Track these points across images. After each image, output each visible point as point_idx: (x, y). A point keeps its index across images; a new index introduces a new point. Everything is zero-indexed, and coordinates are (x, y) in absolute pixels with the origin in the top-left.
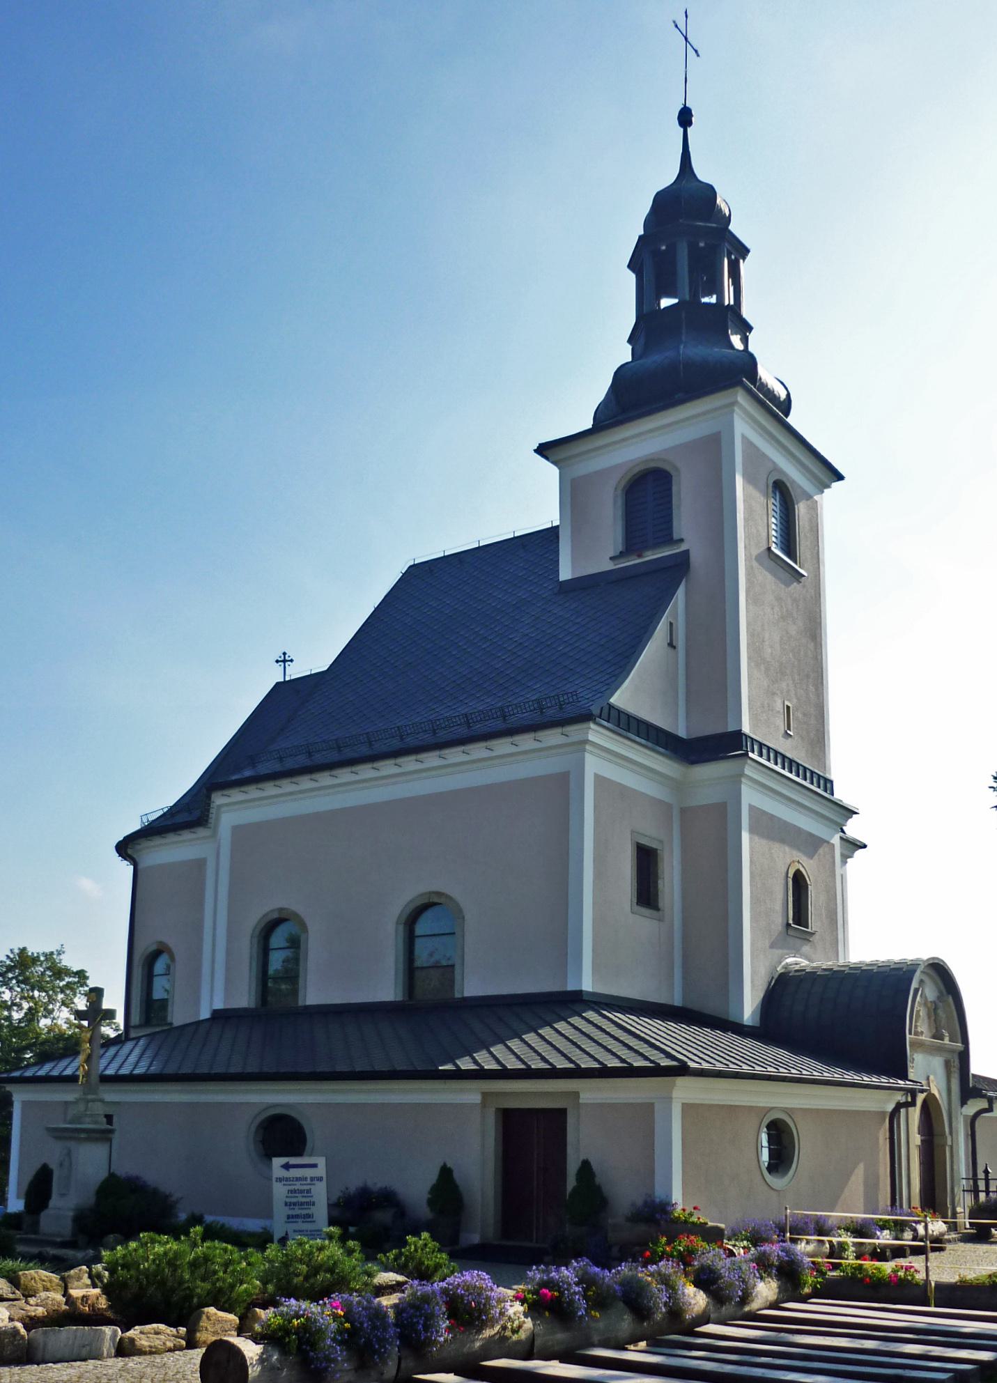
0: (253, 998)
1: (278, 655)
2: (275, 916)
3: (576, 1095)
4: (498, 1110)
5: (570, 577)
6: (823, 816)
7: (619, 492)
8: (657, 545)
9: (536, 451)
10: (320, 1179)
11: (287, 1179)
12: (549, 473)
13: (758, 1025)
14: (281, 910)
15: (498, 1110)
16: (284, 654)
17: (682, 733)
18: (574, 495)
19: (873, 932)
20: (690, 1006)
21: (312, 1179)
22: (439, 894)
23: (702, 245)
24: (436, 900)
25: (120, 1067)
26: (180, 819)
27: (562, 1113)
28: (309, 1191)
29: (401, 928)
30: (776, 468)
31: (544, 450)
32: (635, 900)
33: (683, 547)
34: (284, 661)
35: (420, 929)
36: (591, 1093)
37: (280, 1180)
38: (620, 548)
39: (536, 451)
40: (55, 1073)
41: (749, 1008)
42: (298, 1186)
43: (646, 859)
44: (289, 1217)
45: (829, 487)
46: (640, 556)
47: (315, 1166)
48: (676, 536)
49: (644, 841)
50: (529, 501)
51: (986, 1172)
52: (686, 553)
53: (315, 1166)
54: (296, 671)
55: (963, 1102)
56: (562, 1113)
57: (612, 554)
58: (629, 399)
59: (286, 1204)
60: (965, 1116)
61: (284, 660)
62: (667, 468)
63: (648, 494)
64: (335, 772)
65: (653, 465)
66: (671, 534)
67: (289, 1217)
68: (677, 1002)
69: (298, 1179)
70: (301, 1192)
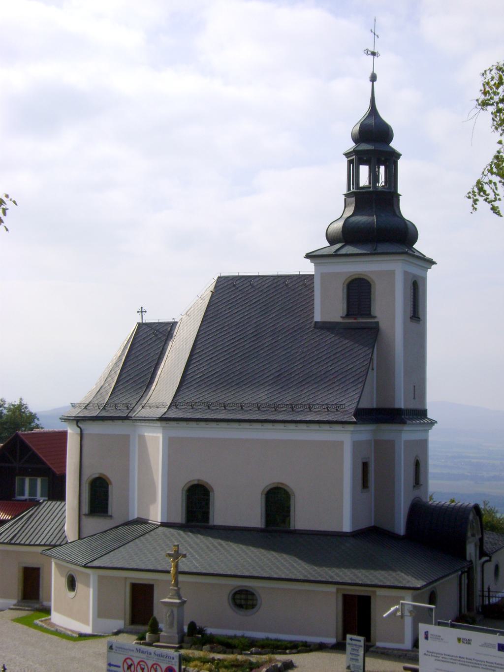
6: (369, 261)
7: (345, 285)
10: (360, 646)
20: (169, 522)
21: (359, 646)
23: (365, 158)
25: (36, 541)
28: (358, 650)
33: (376, 320)
36: (380, 592)
37: (349, 644)
38: (345, 313)
42: (355, 647)
43: (365, 465)
44: (351, 658)
46: (355, 319)
47: (360, 641)
52: (377, 323)
53: (360, 641)
55: (480, 558)
57: (341, 315)
59: (350, 653)
63: (359, 293)
64: (240, 424)
65: (362, 277)
67: (351, 658)
70: (356, 650)
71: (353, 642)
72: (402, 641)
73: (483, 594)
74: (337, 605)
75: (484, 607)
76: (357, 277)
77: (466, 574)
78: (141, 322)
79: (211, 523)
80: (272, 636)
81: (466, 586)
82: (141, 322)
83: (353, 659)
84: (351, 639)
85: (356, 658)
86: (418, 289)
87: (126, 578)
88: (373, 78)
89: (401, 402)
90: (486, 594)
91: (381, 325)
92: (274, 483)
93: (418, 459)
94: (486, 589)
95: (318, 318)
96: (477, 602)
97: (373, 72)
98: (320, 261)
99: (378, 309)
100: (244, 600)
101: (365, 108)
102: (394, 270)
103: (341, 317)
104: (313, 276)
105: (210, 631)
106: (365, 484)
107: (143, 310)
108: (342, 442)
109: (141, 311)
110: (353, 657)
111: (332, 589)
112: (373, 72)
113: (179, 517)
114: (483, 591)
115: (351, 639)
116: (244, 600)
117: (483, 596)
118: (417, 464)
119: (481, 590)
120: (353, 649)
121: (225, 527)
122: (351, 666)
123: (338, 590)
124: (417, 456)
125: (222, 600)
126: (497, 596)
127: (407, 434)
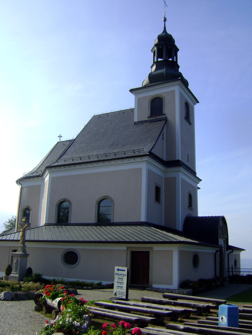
0: (56, 221)
1: (59, 135)
2: (63, 200)
3: (152, 248)
4: (131, 251)
5: (137, 121)
7: (150, 102)
8: (159, 115)
9: (129, 91)
11: (118, 274)
12: (132, 97)
13: (182, 231)
14: (64, 199)
15: (131, 251)
16: (60, 135)
17: (165, 160)
18: (139, 102)
19: (205, 209)
22: (107, 196)
24: (106, 198)
26: (34, 175)
27: (148, 253)
28: (123, 279)
29: (97, 204)
30: (186, 100)
31: (131, 91)
32: (155, 200)
33: (166, 116)
34: (60, 137)
35: (102, 204)
36: (156, 248)
37: (116, 274)
38: (150, 115)
39: (129, 91)
40: (11, 239)
41: (180, 228)
43: (158, 189)
45: (196, 104)
47: (124, 271)
48: (164, 113)
49: (157, 185)
50: (128, 102)
51: (232, 267)
52: (166, 117)
53: (124, 271)
54: (63, 139)
55: (227, 250)
56: (149, 252)
57: (148, 116)
58: (154, 79)
60: (227, 254)
61: (60, 137)
62: (162, 97)
63: (157, 106)
65: (158, 96)
66: (162, 112)
68: (163, 225)
69: (121, 274)
70: (121, 279)
71: (120, 272)
72: (171, 284)
73: (229, 270)
74: (127, 258)
75: (229, 277)
76: (156, 96)
77: (219, 252)
78: (59, 141)
79: (69, 222)
80: (81, 280)
81: (219, 262)
82: (59, 141)
83: (119, 287)
84: (118, 270)
85: (121, 286)
86: (189, 108)
87: (10, 247)
88: (165, 20)
89: (179, 157)
90: (231, 270)
91: (168, 118)
92: (103, 196)
93: (191, 193)
94: (230, 267)
95: (136, 120)
96: (226, 274)
97: (165, 17)
98: (158, 166)
99: (167, 110)
100: (71, 258)
101: (162, 30)
102: (175, 90)
103: (148, 117)
104: (134, 108)
105: (44, 277)
106: (158, 198)
107: (61, 136)
108: (141, 169)
109: (60, 136)
110: (119, 285)
111: (124, 247)
112: (165, 17)
113: (54, 221)
114: (229, 268)
115: (118, 270)
116: (71, 258)
117: (229, 271)
118: (190, 197)
119: (228, 268)
120: (119, 278)
121: (100, 243)
122: (117, 293)
123: (127, 248)
124: (189, 192)
125: (58, 259)
126: (237, 271)
127: (182, 175)
